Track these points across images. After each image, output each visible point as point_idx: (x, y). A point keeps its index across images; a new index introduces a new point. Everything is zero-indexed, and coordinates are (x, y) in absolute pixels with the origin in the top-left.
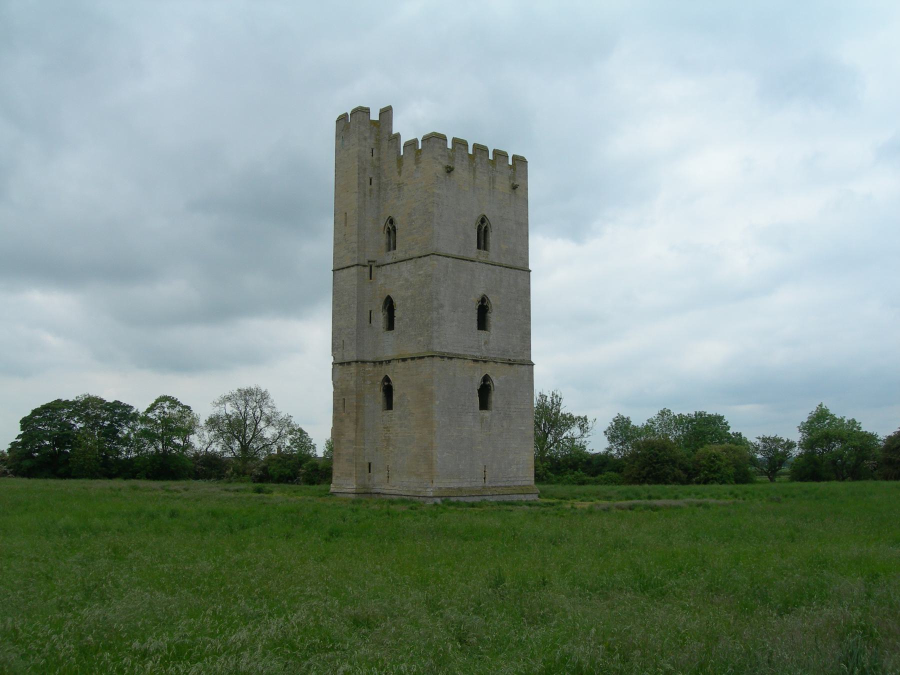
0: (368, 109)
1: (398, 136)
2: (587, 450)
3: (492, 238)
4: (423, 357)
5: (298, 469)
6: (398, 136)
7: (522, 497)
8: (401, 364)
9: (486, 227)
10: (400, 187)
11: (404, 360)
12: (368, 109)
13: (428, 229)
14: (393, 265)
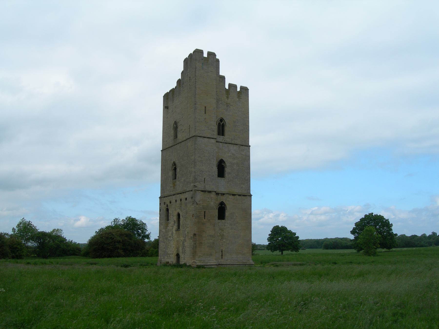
2: (62, 236)
3: (227, 129)
4: (246, 196)
7: (280, 263)
8: (231, 197)
9: (223, 124)
10: (228, 105)
11: (234, 195)
13: (206, 116)
14: (224, 144)
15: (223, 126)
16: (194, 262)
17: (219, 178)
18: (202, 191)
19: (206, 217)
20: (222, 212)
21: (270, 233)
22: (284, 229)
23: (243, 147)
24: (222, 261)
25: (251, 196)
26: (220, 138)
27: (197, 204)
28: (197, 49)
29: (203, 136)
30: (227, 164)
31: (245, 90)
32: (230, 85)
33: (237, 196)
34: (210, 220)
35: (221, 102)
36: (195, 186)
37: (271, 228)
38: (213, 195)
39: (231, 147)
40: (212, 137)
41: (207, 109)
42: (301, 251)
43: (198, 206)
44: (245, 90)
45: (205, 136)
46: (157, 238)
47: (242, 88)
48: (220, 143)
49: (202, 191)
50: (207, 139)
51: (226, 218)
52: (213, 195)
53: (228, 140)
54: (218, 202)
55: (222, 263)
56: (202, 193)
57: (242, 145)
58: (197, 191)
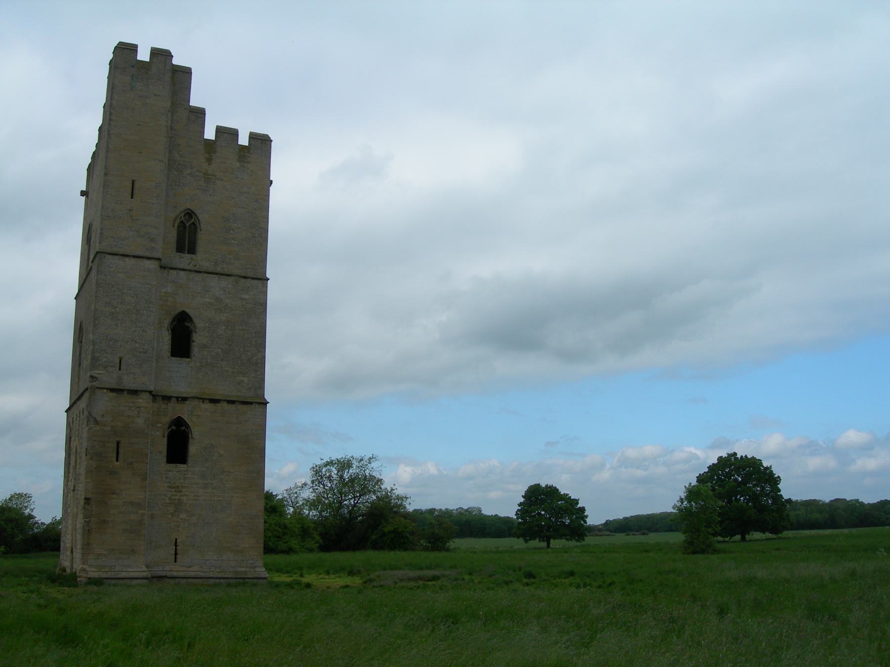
0: (136, 46)
1: (200, 113)
4: (251, 403)
5: (48, 540)
6: (200, 113)
8: (207, 406)
11: (214, 401)
12: (136, 46)
14: (193, 275)
15: (194, 228)
16: (84, 570)
17: (173, 358)
18: (112, 390)
19: (120, 456)
20: (178, 445)
21: (522, 500)
22: (551, 492)
23: (249, 282)
24: (177, 570)
25: (265, 403)
26: (184, 260)
27: (96, 422)
28: (120, 43)
29: (122, 251)
30: (199, 323)
31: (261, 143)
32: (220, 130)
33: (225, 405)
34: (131, 463)
35: (189, 171)
36: (92, 377)
37: (523, 489)
38: (144, 401)
39: (213, 281)
40: (148, 254)
41: (136, 185)
42: (589, 540)
43: (98, 428)
44: (261, 143)
45: (128, 253)
46: (594, 518)
47: (253, 137)
48: (182, 273)
49: (112, 390)
50: (133, 260)
51: (190, 460)
52: (144, 401)
53: (206, 265)
54: (166, 420)
55: (175, 574)
56: (112, 394)
57: (245, 277)
58: (98, 391)
